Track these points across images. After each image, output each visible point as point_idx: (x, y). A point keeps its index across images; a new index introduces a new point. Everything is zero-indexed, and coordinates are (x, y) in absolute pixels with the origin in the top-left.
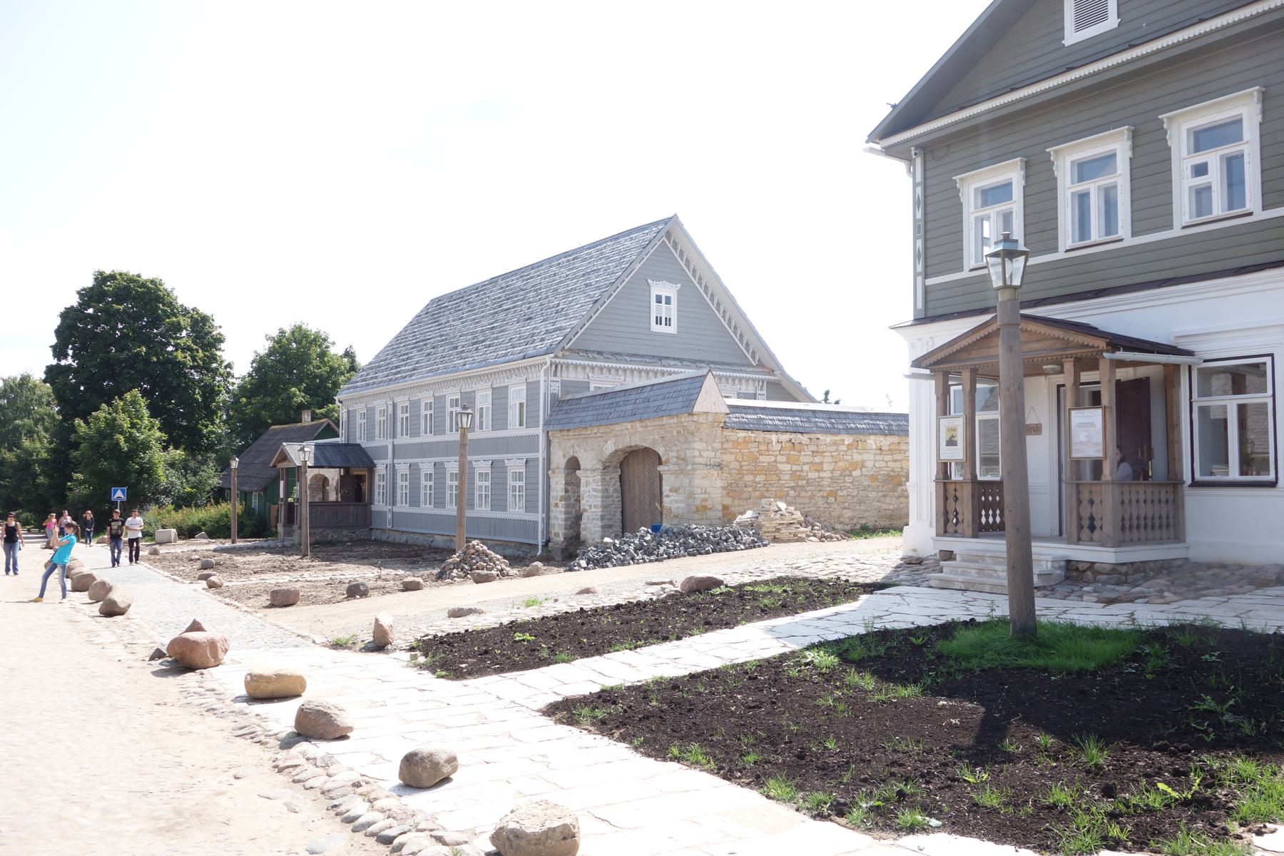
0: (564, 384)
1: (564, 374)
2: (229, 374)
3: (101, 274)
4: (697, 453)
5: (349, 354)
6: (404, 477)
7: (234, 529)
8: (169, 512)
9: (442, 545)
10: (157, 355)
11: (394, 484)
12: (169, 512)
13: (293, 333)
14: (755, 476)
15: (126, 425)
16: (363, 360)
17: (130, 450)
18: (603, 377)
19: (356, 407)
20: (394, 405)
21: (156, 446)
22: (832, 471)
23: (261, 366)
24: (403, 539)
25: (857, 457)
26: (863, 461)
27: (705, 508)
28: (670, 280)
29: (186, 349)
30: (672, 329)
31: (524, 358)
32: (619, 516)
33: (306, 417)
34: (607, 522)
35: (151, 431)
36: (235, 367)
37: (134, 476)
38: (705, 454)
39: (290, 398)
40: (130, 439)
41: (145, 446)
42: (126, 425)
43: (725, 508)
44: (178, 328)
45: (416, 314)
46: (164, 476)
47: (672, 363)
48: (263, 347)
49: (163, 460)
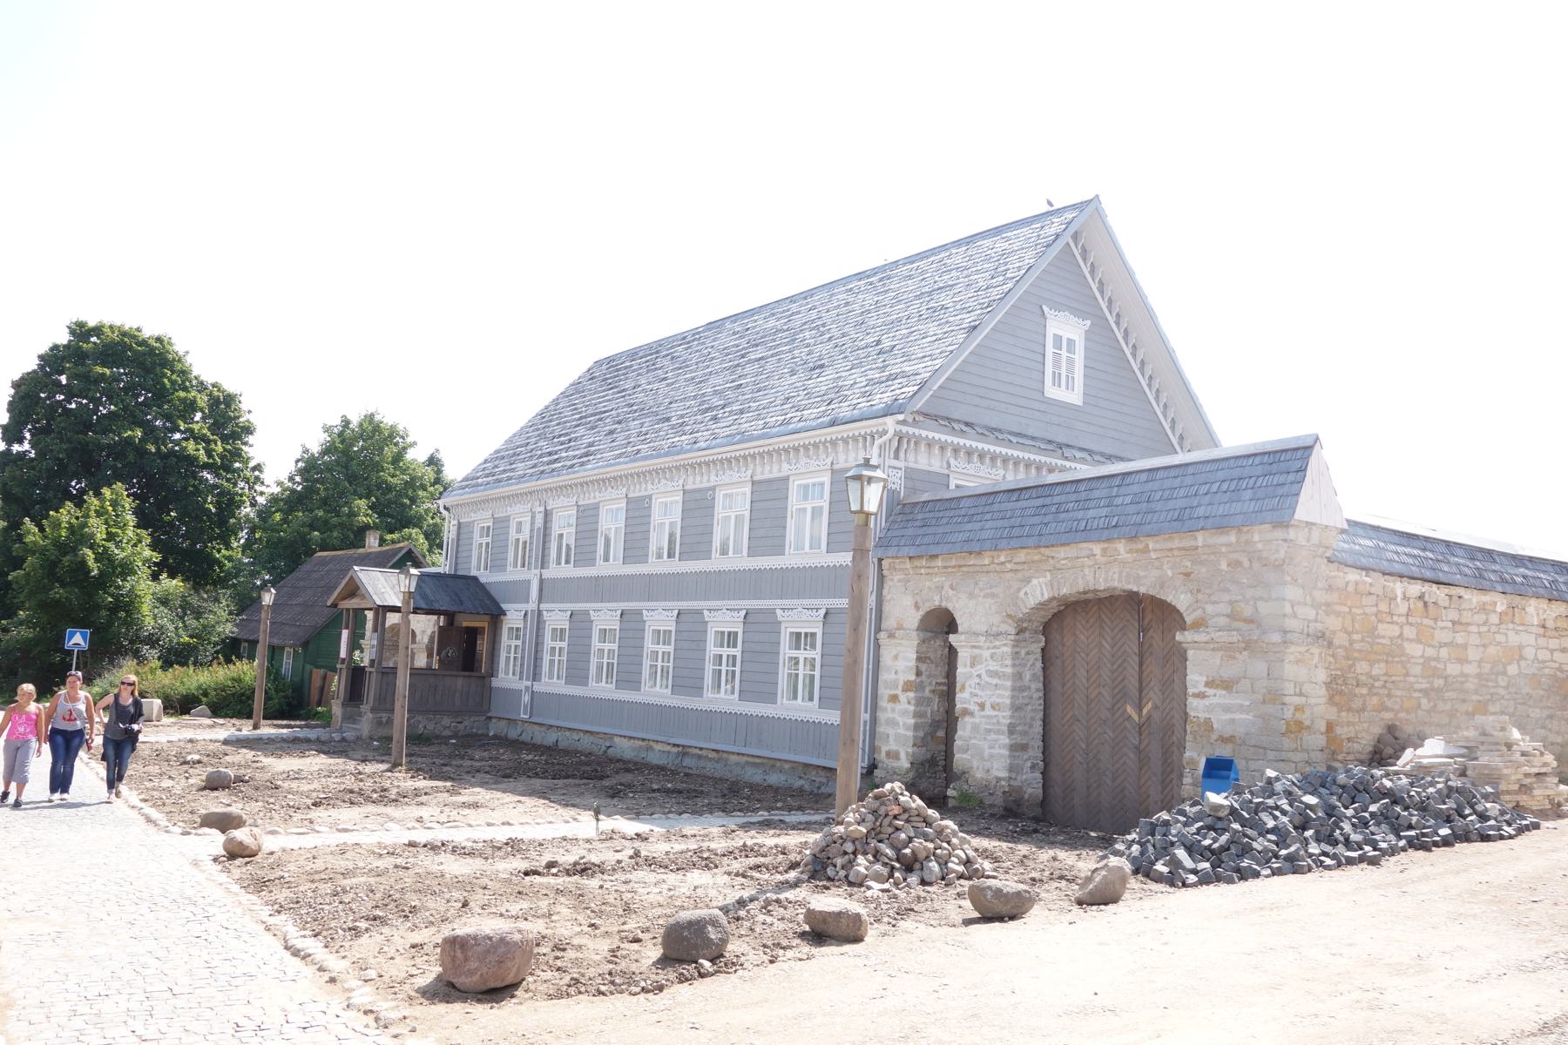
0: (910, 474)
1: (911, 457)
2: (257, 478)
3: (81, 325)
4: (1288, 610)
5: (433, 461)
6: (559, 634)
7: (258, 704)
8: (152, 671)
9: (628, 755)
10: (156, 443)
11: (538, 644)
12: (152, 671)
13: (361, 425)
14: (1372, 663)
15: (100, 535)
16: (454, 471)
17: (101, 573)
18: (971, 469)
19: (474, 516)
20: (547, 515)
21: (144, 572)
22: (1480, 662)
23: (309, 468)
24: (550, 738)
25: (1514, 639)
26: (1521, 647)
27: (1300, 726)
28: (1076, 312)
29: (198, 438)
30: (1075, 397)
31: (833, 423)
32: (1038, 727)
33: (372, 541)
34: (1019, 739)
35: (137, 548)
36: (266, 470)
37: (104, 613)
38: (1300, 611)
39: (353, 514)
40: (103, 557)
41: (127, 569)
42: (100, 535)
43: (1330, 727)
44: (191, 406)
45: (538, 406)
46: (150, 616)
47: (1079, 455)
48: (315, 442)
49: (152, 594)
